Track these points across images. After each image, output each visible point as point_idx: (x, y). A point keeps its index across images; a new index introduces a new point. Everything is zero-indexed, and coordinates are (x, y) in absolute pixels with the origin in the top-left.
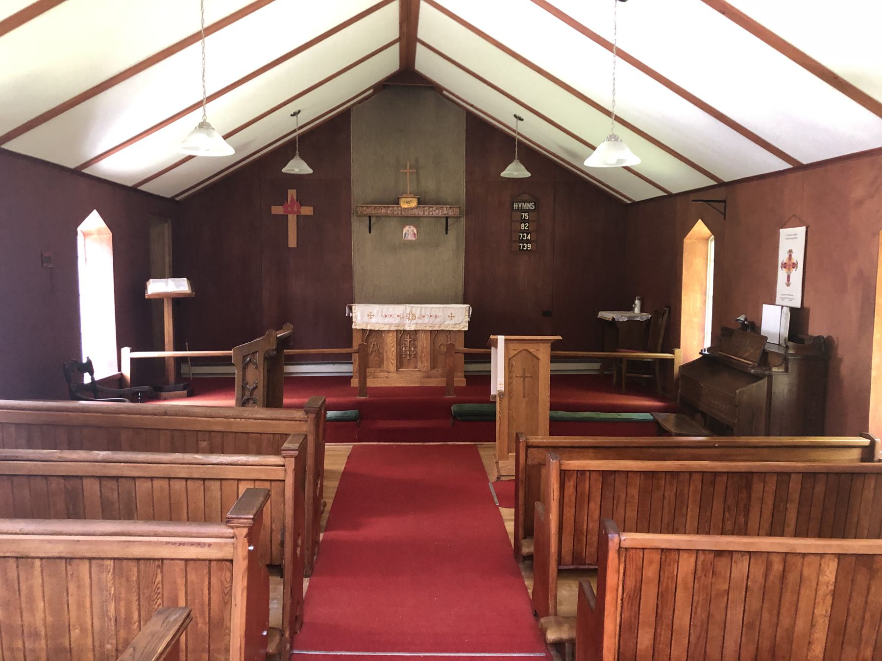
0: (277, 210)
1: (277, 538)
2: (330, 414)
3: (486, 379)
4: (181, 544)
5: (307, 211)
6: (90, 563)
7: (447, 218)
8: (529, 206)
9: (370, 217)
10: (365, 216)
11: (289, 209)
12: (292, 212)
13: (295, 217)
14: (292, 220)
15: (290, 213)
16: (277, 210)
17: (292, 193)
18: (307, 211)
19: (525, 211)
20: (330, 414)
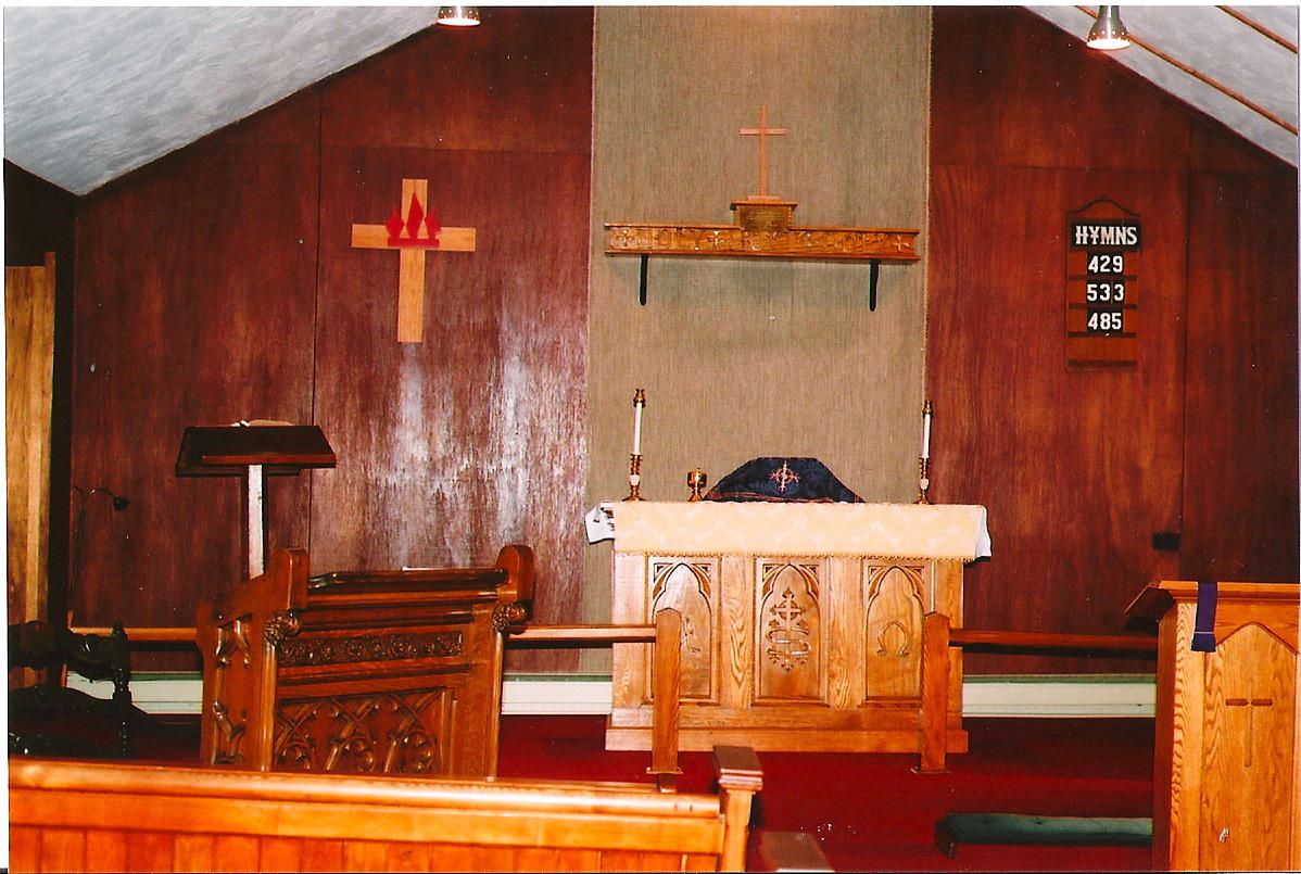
0: (371, 235)
1: (893, 604)
2: (168, 696)
3: (280, 660)
4: (754, 637)
5: (457, 238)
6: (85, 835)
7: (645, 257)
8: (1122, 235)
9: (645, 257)
10: (628, 253)
11: (404, 233)
12: (413, 241)
13: (422, 257)
14: (412, 261)
15: (405, 243)
16: (371, 235)
17: (415, 189)
18: (457, 238)
19: (1112, 250)
20: (168, 696)
